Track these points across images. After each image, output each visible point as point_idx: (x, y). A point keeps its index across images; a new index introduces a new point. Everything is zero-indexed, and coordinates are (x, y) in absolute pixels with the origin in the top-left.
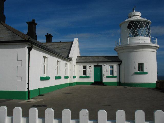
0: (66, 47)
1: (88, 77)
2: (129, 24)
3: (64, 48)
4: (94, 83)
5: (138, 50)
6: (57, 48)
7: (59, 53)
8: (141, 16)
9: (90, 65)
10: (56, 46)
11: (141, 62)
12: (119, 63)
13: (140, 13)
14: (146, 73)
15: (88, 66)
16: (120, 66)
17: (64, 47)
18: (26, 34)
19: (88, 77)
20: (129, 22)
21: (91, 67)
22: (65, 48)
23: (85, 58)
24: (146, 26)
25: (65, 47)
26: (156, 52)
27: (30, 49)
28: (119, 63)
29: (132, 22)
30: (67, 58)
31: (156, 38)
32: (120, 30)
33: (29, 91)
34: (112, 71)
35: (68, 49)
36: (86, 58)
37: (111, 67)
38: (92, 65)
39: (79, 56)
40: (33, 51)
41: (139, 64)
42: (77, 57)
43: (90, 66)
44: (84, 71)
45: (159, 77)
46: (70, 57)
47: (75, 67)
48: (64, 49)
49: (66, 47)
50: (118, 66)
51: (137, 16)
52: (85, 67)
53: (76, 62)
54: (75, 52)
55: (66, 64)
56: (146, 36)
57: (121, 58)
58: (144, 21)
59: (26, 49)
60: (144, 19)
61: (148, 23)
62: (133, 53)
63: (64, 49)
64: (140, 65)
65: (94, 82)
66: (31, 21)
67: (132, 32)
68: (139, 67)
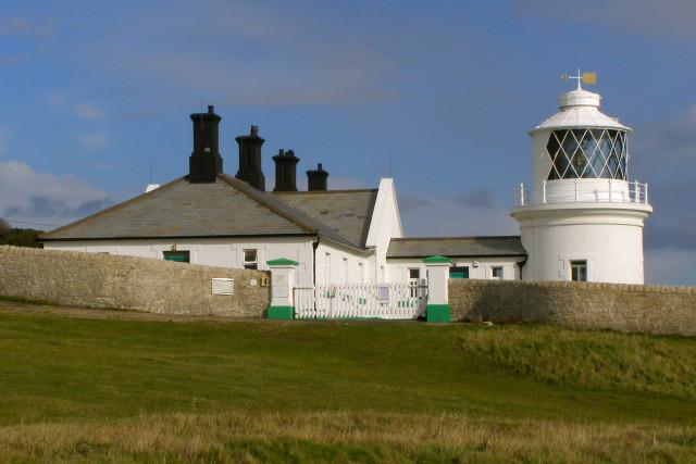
3: (348, 212)
5: (558, 222)
6: (325, 213)
7: (336, 230)
8: (603, 108)
10: (324, 207)
11: (578, 257)
12: (521, 260)
16: (524, 269)
25: (352, 209)
27: (315, 246)
28: (521, 260)
29: (560, 132)
30: (361, 248)
32: (598, 104)
35: (360, 218)
39: (399, 235)
40: (322, 248)
41: (574, 263)
46: (368, 244)
47: (383, 273)
48: (348, 215)
50: (518, 269)
51: (586, 110)
53: (388, 258)
54: (386, 224)
55: (360, 264)
56: (602, 177)
57: (527, 244)
59: (310, 245)
62: (557, 229)
63: (348, 215)
64: (579, 267)
66: (247, 133)
68: (574, 271)
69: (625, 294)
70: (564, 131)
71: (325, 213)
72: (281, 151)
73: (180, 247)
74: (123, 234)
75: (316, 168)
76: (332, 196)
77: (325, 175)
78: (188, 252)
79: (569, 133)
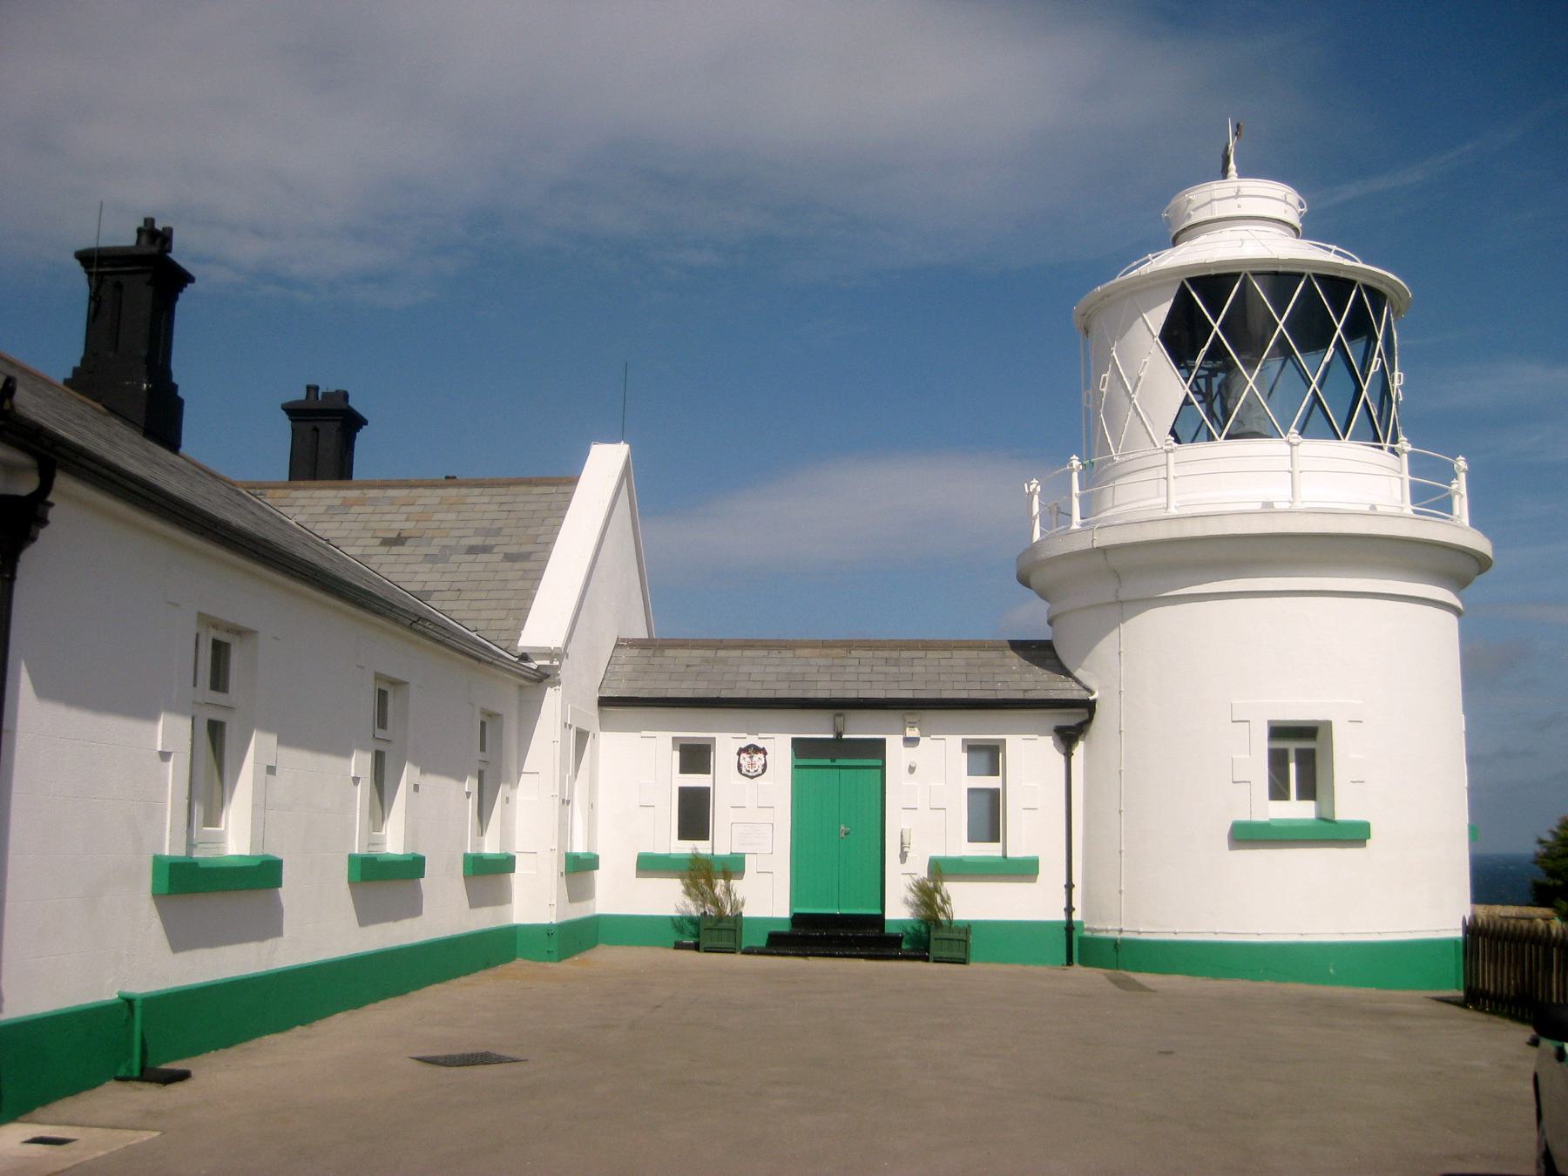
0: (498, 532)
1: (1025, 870)
2: (1182, 300)
3: (477, 541)
4: (786, 928)
6: (399, 540)
8: (1309, 229)
9: (752, 740)
10: (397, 523)
12: (1070, 719)
13: (1293, 196)
14: (1355, 835)
15: (726, 745)
17: (477, 532)
18: (67, 382)
19: (1025, 870)
20: (1177, 287)
21: (758, 758)
22: (486, 549)
23: (707, 660)
24: (1360, 327)
25: (487, 533)
26: (1299, 225)
28: (1070, 719)
31: (1461, 463)
33: (1070, 927)
34: (985, 801)
36: (709, 653)
37: (983, 758)
38: (779, 747)
39: (641, 633)
41: (1279, 732)
42: (618, 645)
43: (753, 750)
44: (684, 792)
45: (967, 928)
48: (472, 550)
49: (498, 532)
52: (695, 757)
53: (604, 702)
58: (1337, 285)
60: (1331, 258)
61: (1378, 297)
63: (472, 550)
64: (1292, 746)
65: (797, 919)
66: (123, 236)
67: (1207, 399)
68: (1277, 761)
69: (900, 923)
70: (1229, 279)
71: (399, 540)
72: (312, 389)
73: (858, 729)
74: (757, 692)
75: (302, 395)
76: (181, 461)
77: (351, 422)
78: (715, 738)
79: (1309, 289)
